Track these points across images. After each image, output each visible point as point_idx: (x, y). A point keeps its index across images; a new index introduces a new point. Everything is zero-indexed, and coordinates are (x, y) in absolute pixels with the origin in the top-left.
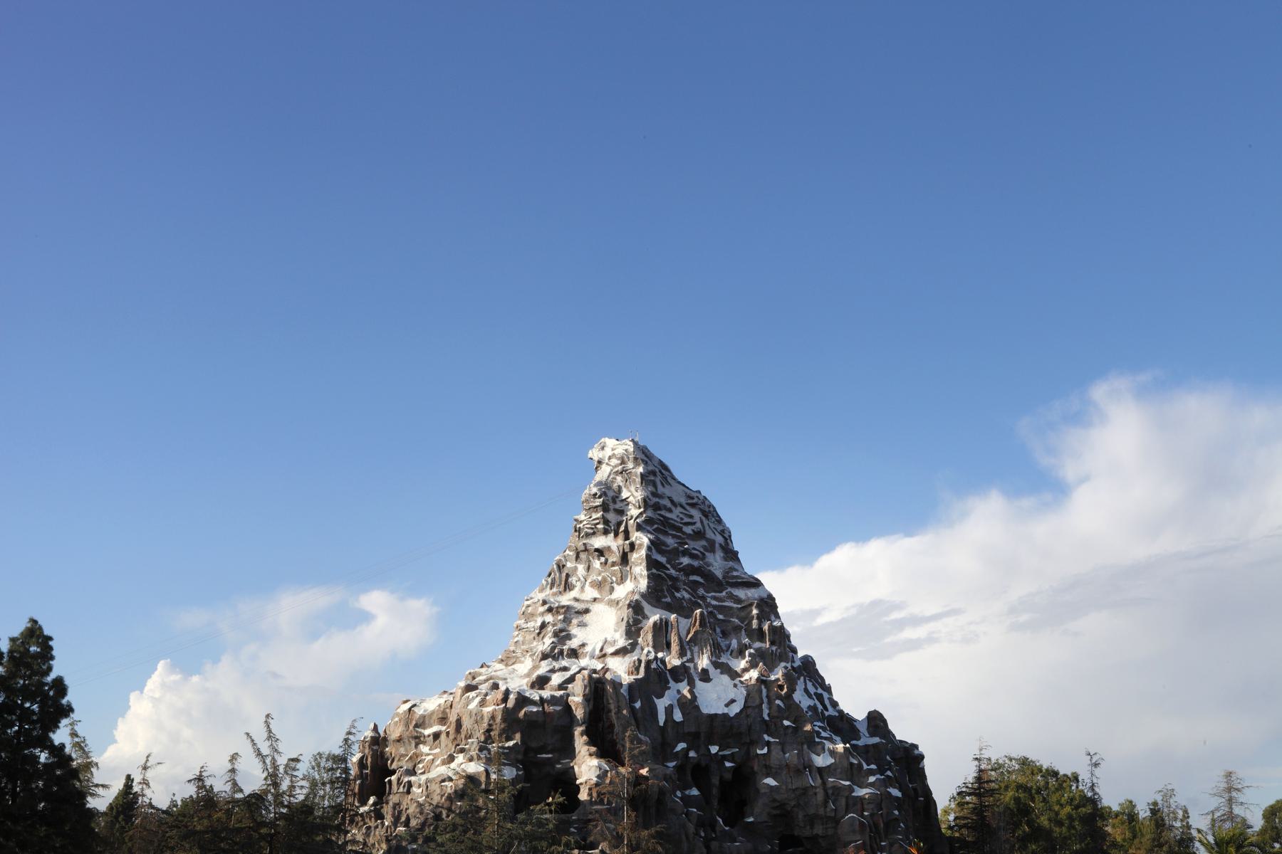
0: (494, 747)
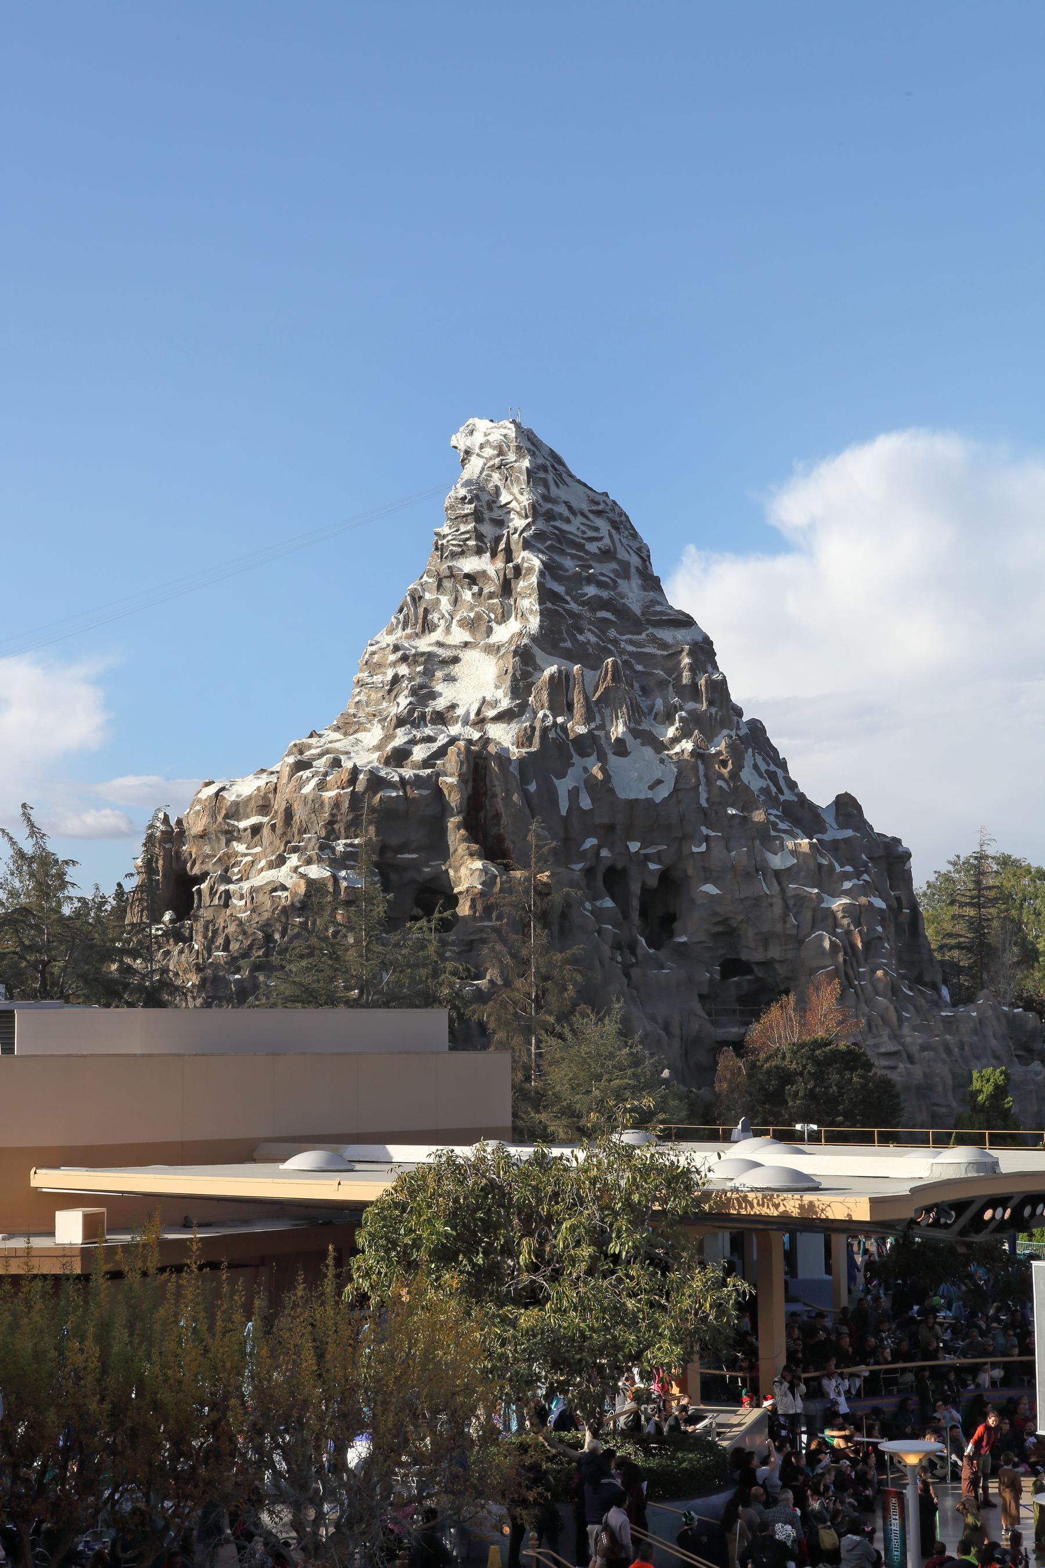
0: (340, 845)
